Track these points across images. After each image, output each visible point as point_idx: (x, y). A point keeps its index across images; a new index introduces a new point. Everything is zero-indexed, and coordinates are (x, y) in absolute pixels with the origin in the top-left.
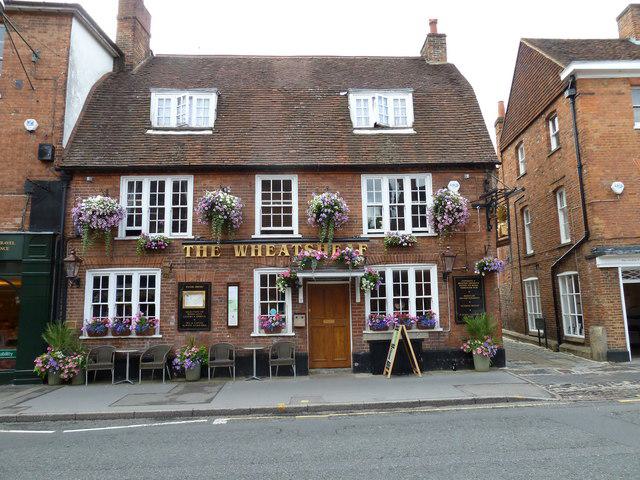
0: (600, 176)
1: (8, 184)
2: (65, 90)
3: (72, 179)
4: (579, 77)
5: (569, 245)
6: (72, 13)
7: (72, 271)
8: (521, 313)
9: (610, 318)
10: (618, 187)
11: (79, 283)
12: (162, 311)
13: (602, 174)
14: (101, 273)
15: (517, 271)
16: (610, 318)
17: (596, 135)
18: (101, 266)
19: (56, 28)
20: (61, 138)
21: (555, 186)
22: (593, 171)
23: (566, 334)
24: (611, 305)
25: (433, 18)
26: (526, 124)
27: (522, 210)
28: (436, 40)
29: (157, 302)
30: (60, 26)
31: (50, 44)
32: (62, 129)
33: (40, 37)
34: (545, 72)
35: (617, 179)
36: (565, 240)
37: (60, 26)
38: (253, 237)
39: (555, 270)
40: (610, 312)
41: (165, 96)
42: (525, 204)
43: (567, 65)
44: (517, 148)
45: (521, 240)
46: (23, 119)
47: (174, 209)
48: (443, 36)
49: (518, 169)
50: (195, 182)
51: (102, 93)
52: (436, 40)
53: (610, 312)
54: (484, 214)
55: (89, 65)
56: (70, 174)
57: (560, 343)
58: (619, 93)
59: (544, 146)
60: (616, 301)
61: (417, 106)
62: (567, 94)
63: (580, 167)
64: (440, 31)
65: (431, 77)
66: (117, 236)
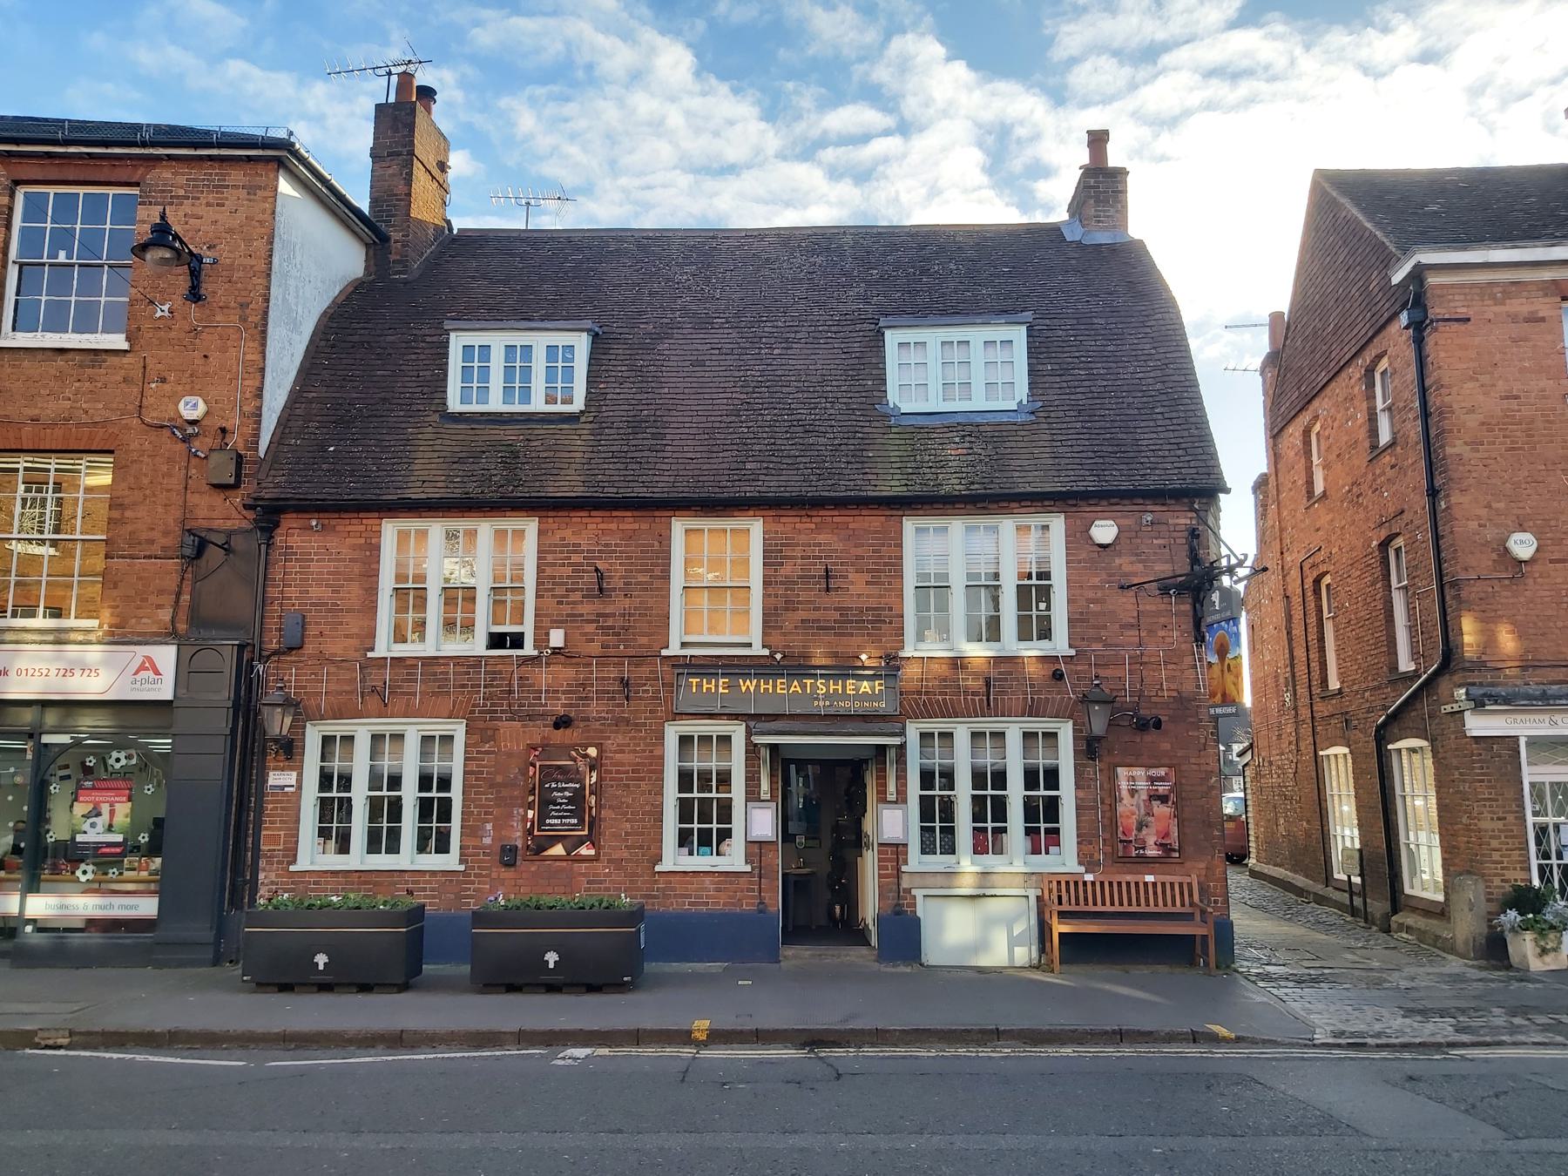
0: (1479, 518)
1: (144, 536)
2: (264, 332)
3: (277, 525)
4: (1433, 280)
5: (1415, 675)
6: (277, 154)
7: (278, 723)
8: (1317, 835)
9: (1496, 856)
10: (1523, 546)
11: (290, 750)
12: (465, 814)
13: (1483, 512)
14: (338, 728)
15: (1306, 730)
16: (1496, 856)
17: (1472, 421)
18: (338, 714)
19: (243, 193)
20: (257, 436)
21: (1384, 534)
22: (1464, 504)
23: (1407, 891)
24: (1500, 824)
25: (1096, 126)
26: (1323, 377)
27: (1317, 581)
28: (1102, 185)
29: (456, 794)
30: (252, 189)
31: (230, 231)
32: (258, 415)
33: (211, 214)
34: (1385, 253)
35: (1522, 528)
36: (1405, 664)
37: (252, 189)
38: (664, 652)
39: (1382, 736)
40: (1495, 843)
41: (476, 339)
42: (1323, 568)
43: (1406, 251)
44: (1307, 433)
45: (1314, 655)
46: (175, 398)
47: (323, 801)
48: (1119, 175)
49: (1310, 483)
50: (540, 533)
51: (347, 327)
52: (1102, 185)
53: (1495, 843)
54: (1187, 607)
55: (314, 264)
56: (269, 515)
57: (1395, 911)
58: (1534, 319)
59: (1362, 434)
60: (1511, 818)
61: (1035, 352)
62: (1404, 318)
63: (1433, 493)
64: (1113, 162)
65: (1078, 288)
66: (372, 649)
